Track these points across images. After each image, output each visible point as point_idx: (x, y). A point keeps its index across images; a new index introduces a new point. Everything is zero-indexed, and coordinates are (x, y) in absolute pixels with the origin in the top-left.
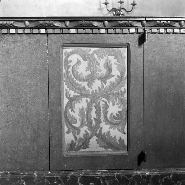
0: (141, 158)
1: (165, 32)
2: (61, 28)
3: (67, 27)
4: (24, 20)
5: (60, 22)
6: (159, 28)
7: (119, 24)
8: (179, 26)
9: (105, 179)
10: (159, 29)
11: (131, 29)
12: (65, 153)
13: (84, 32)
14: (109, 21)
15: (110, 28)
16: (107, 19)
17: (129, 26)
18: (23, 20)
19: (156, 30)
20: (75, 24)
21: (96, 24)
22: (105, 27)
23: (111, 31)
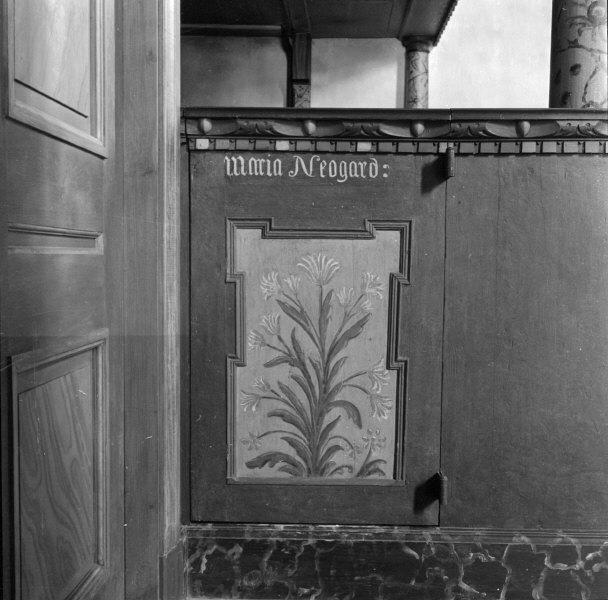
0: (429, 491)
1: (539, 151)
2: (291, 139)
3: (307, 136)
4: (304, 116)
5: (507, 125)
6: (236, 140)
7: (241, 129)
8: (302, 134)
9: (563, 567)
10: (584, 144)
11: (278, 143)
12: (241, 473)
13: (251, 148)
14: (532, 122)
15: (426, 140)
16: (527, 117)
17: (481, 137)
18: (229, 115)
19: (247, 142)
20: (227, 128)
21: (493, 129)
22: (415, 139)
23: (324, 146)
